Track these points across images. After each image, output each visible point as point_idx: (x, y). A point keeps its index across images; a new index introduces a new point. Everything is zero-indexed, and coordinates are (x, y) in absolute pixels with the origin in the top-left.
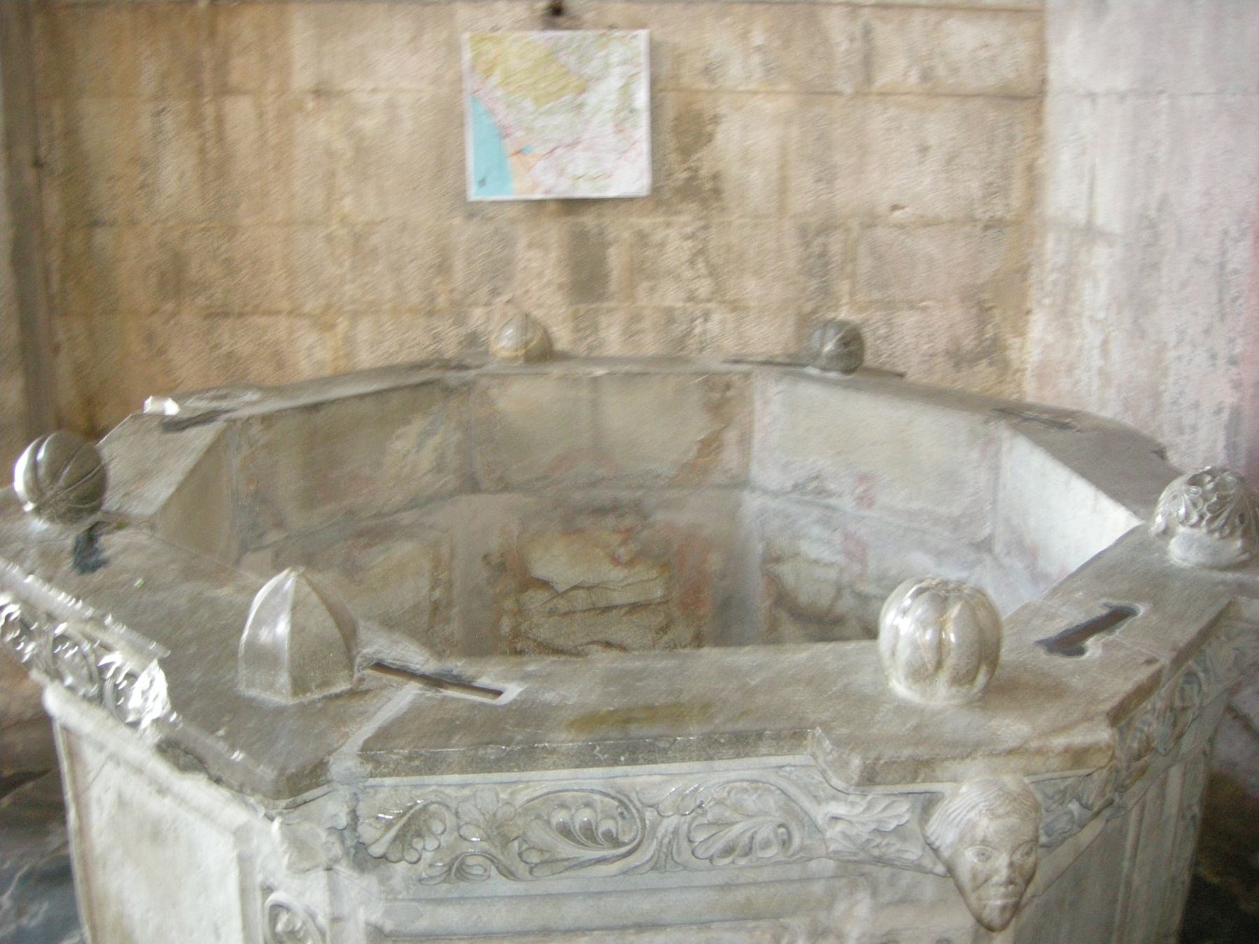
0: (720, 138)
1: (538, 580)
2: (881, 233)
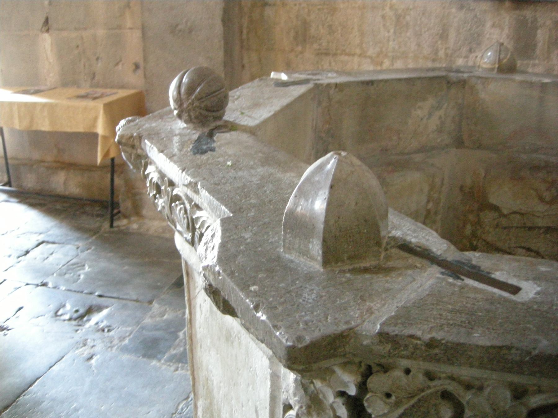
1: (492, 205)
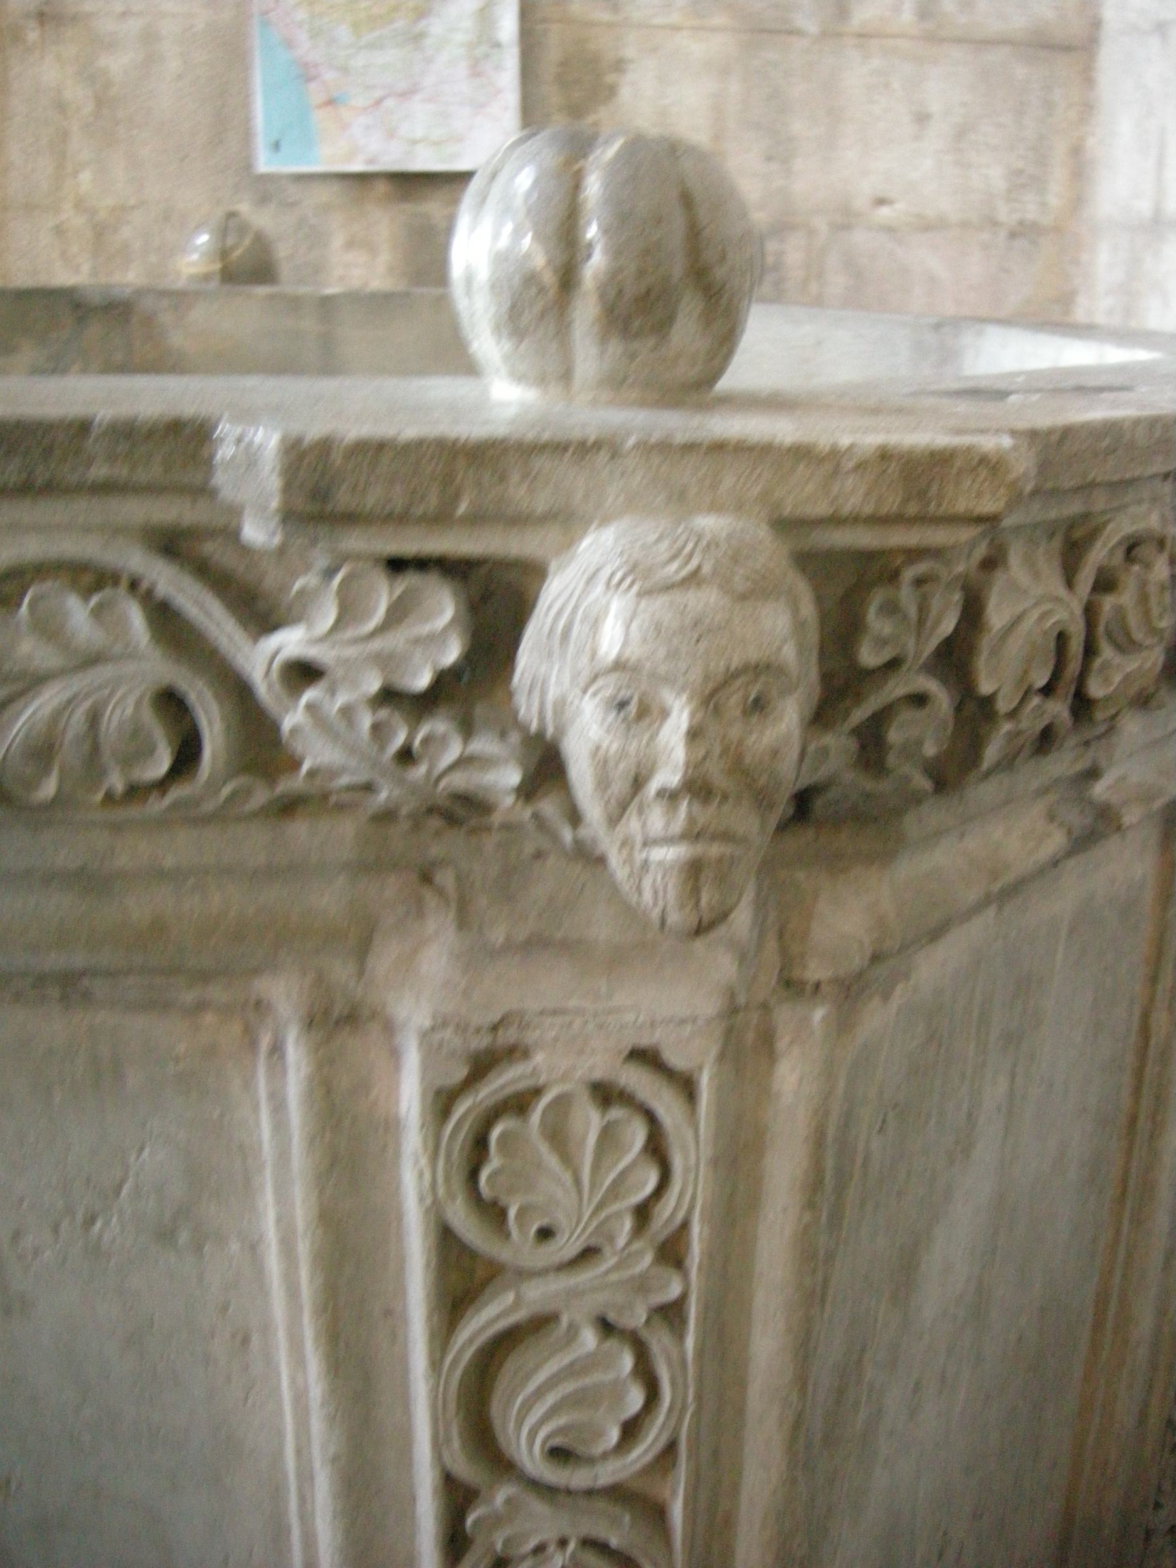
0: (625, 93)
2: (860, 238)
